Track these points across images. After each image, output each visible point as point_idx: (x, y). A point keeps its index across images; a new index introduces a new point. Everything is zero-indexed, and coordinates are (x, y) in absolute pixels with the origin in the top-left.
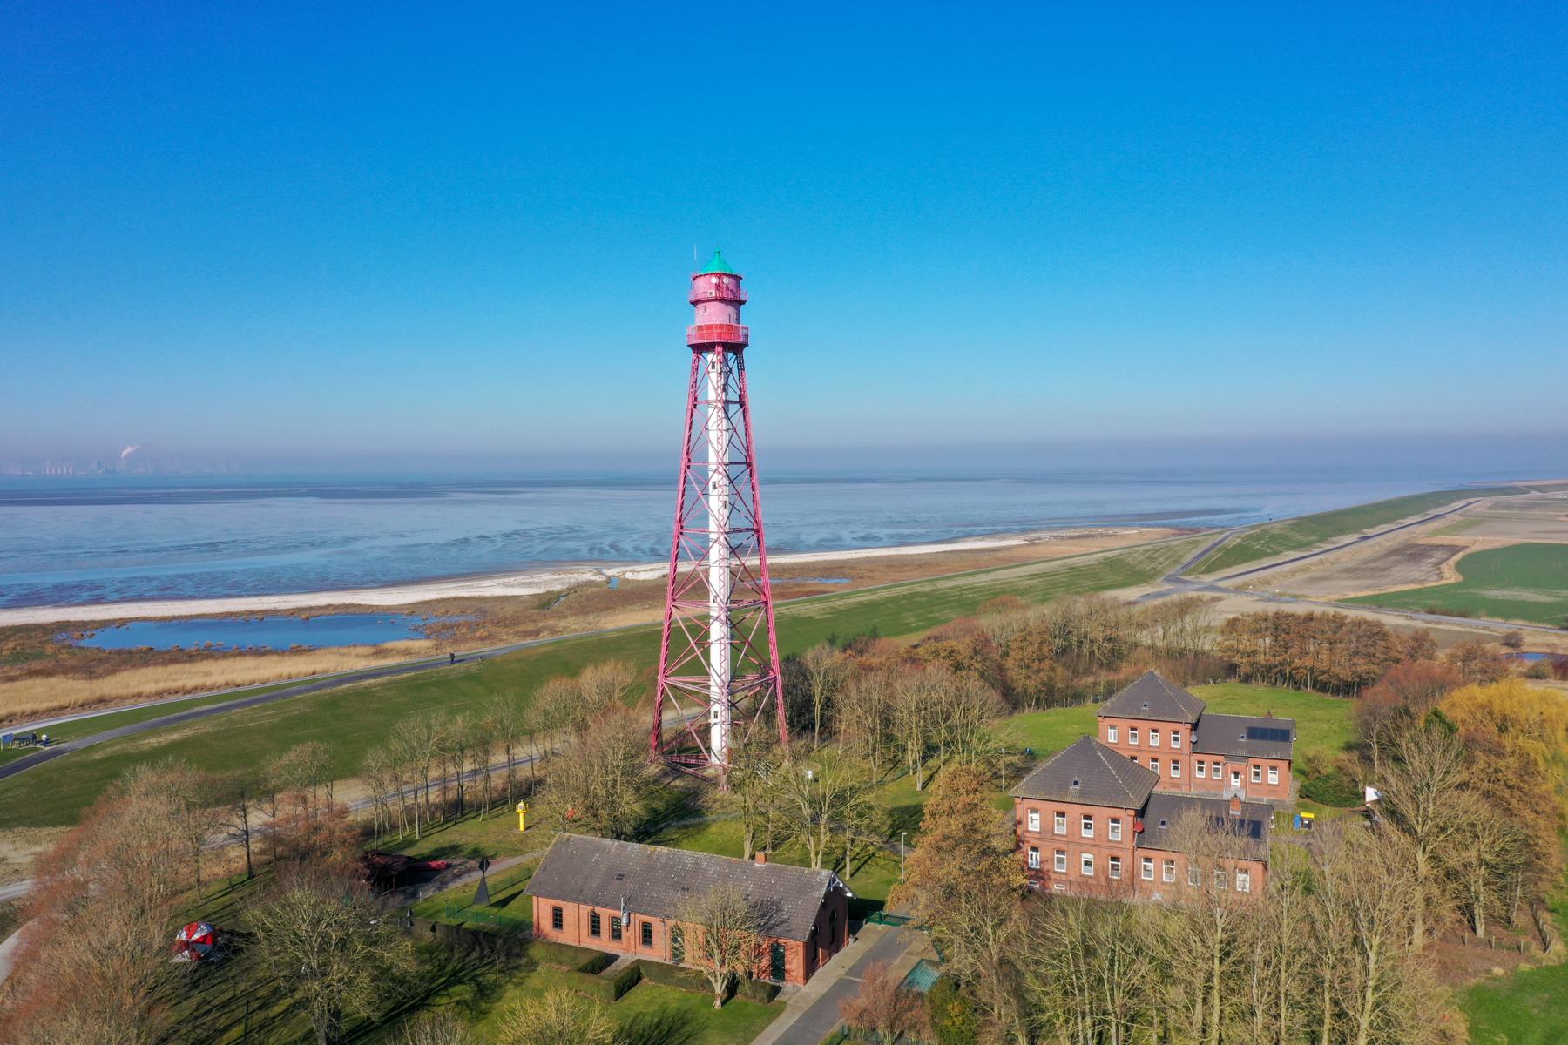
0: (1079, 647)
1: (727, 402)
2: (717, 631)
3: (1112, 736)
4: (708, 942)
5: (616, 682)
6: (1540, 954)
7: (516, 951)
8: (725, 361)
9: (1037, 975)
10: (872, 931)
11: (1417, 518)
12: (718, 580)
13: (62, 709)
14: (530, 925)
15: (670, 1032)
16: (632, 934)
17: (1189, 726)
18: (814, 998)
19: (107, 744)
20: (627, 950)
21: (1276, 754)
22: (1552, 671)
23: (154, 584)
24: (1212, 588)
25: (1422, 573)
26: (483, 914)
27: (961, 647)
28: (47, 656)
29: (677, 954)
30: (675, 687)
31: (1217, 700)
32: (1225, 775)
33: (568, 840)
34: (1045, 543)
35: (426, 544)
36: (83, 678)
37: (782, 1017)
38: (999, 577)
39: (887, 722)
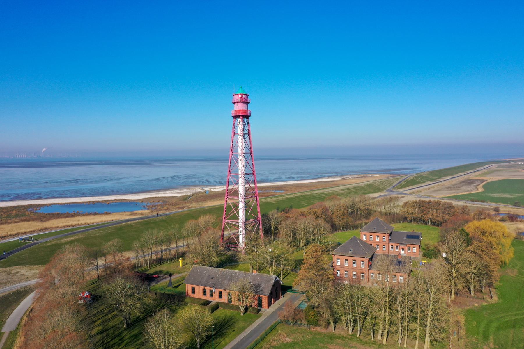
0: (357, 212)
1: (244, 134)
2: (241, 206)
3: (364, 238)
4: (239, 295)
5: (210, 221)
6: (489, 300)
7: (181, 300)
8: (243, 121)
9: (336, 304)
10: (288, 295)
12: (241, 189)
13: (34, 231)
14: (185, 293)
15: (228, 321)
16: (216, 295)
17: (388, 234)
18: (271, 312)
19: (51, 241)
20: (214, 300)
21: (415, 243)
22: (508, 219)
23: (58, 193)
24: (402, 193)
26: (170, 290)
27: (318, 211)
28: (27, 215)
29: (230, 301)
30: (228, 223)
32: (399, 249)
33: (196, 267)
34: (348, 179)
36: (39, 222)
37: (261, 318)
38: (332, 190)
39: (294, 234)
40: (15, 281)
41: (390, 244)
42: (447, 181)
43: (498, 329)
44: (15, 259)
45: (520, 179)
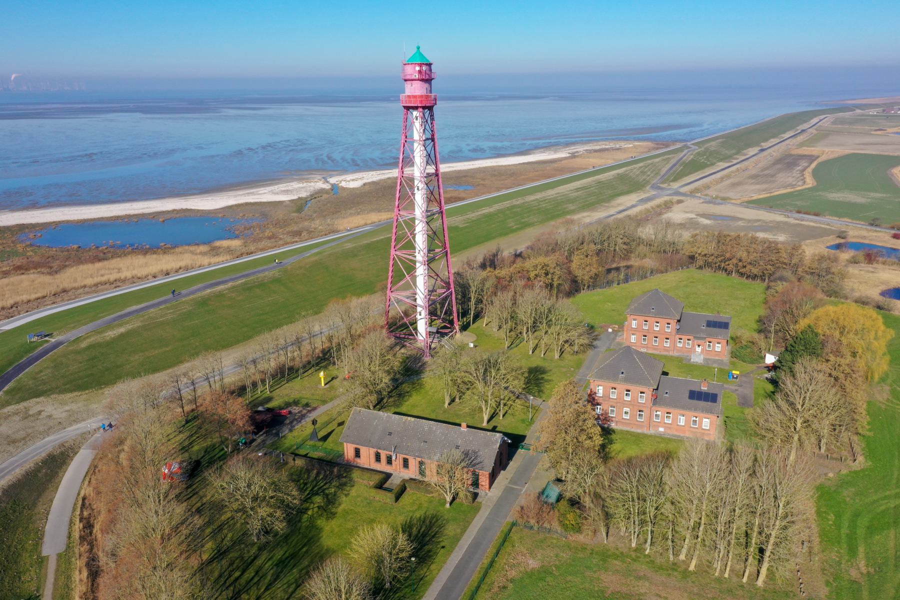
8: (423, 117)
11: (791, 133)
16: (397, 462)
18: (495, 499)
25: (794, 179)
29: (422, 473)
31: (685, 283)
32: (693, 346)
35: (218, 156)
40: (40, 433)
41: (678, 336)
42: (751, 160)
43: (871, 530)
44: (30, 382)
45: (874, 153)
